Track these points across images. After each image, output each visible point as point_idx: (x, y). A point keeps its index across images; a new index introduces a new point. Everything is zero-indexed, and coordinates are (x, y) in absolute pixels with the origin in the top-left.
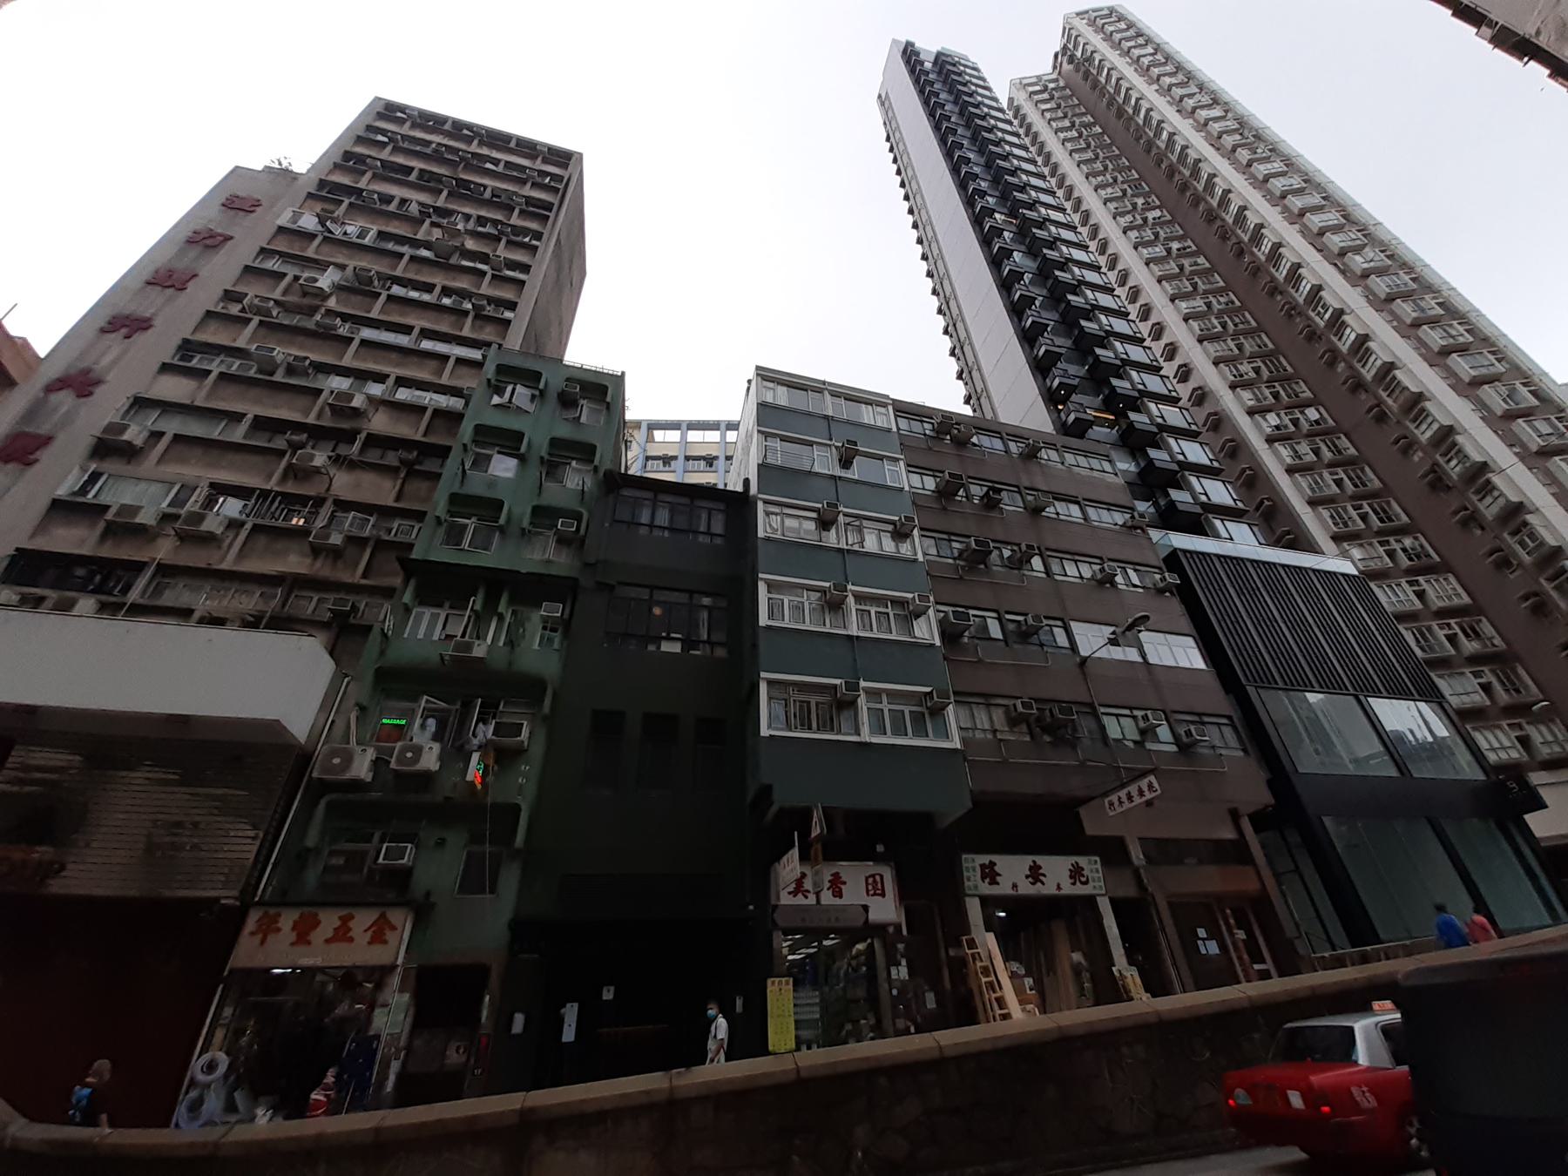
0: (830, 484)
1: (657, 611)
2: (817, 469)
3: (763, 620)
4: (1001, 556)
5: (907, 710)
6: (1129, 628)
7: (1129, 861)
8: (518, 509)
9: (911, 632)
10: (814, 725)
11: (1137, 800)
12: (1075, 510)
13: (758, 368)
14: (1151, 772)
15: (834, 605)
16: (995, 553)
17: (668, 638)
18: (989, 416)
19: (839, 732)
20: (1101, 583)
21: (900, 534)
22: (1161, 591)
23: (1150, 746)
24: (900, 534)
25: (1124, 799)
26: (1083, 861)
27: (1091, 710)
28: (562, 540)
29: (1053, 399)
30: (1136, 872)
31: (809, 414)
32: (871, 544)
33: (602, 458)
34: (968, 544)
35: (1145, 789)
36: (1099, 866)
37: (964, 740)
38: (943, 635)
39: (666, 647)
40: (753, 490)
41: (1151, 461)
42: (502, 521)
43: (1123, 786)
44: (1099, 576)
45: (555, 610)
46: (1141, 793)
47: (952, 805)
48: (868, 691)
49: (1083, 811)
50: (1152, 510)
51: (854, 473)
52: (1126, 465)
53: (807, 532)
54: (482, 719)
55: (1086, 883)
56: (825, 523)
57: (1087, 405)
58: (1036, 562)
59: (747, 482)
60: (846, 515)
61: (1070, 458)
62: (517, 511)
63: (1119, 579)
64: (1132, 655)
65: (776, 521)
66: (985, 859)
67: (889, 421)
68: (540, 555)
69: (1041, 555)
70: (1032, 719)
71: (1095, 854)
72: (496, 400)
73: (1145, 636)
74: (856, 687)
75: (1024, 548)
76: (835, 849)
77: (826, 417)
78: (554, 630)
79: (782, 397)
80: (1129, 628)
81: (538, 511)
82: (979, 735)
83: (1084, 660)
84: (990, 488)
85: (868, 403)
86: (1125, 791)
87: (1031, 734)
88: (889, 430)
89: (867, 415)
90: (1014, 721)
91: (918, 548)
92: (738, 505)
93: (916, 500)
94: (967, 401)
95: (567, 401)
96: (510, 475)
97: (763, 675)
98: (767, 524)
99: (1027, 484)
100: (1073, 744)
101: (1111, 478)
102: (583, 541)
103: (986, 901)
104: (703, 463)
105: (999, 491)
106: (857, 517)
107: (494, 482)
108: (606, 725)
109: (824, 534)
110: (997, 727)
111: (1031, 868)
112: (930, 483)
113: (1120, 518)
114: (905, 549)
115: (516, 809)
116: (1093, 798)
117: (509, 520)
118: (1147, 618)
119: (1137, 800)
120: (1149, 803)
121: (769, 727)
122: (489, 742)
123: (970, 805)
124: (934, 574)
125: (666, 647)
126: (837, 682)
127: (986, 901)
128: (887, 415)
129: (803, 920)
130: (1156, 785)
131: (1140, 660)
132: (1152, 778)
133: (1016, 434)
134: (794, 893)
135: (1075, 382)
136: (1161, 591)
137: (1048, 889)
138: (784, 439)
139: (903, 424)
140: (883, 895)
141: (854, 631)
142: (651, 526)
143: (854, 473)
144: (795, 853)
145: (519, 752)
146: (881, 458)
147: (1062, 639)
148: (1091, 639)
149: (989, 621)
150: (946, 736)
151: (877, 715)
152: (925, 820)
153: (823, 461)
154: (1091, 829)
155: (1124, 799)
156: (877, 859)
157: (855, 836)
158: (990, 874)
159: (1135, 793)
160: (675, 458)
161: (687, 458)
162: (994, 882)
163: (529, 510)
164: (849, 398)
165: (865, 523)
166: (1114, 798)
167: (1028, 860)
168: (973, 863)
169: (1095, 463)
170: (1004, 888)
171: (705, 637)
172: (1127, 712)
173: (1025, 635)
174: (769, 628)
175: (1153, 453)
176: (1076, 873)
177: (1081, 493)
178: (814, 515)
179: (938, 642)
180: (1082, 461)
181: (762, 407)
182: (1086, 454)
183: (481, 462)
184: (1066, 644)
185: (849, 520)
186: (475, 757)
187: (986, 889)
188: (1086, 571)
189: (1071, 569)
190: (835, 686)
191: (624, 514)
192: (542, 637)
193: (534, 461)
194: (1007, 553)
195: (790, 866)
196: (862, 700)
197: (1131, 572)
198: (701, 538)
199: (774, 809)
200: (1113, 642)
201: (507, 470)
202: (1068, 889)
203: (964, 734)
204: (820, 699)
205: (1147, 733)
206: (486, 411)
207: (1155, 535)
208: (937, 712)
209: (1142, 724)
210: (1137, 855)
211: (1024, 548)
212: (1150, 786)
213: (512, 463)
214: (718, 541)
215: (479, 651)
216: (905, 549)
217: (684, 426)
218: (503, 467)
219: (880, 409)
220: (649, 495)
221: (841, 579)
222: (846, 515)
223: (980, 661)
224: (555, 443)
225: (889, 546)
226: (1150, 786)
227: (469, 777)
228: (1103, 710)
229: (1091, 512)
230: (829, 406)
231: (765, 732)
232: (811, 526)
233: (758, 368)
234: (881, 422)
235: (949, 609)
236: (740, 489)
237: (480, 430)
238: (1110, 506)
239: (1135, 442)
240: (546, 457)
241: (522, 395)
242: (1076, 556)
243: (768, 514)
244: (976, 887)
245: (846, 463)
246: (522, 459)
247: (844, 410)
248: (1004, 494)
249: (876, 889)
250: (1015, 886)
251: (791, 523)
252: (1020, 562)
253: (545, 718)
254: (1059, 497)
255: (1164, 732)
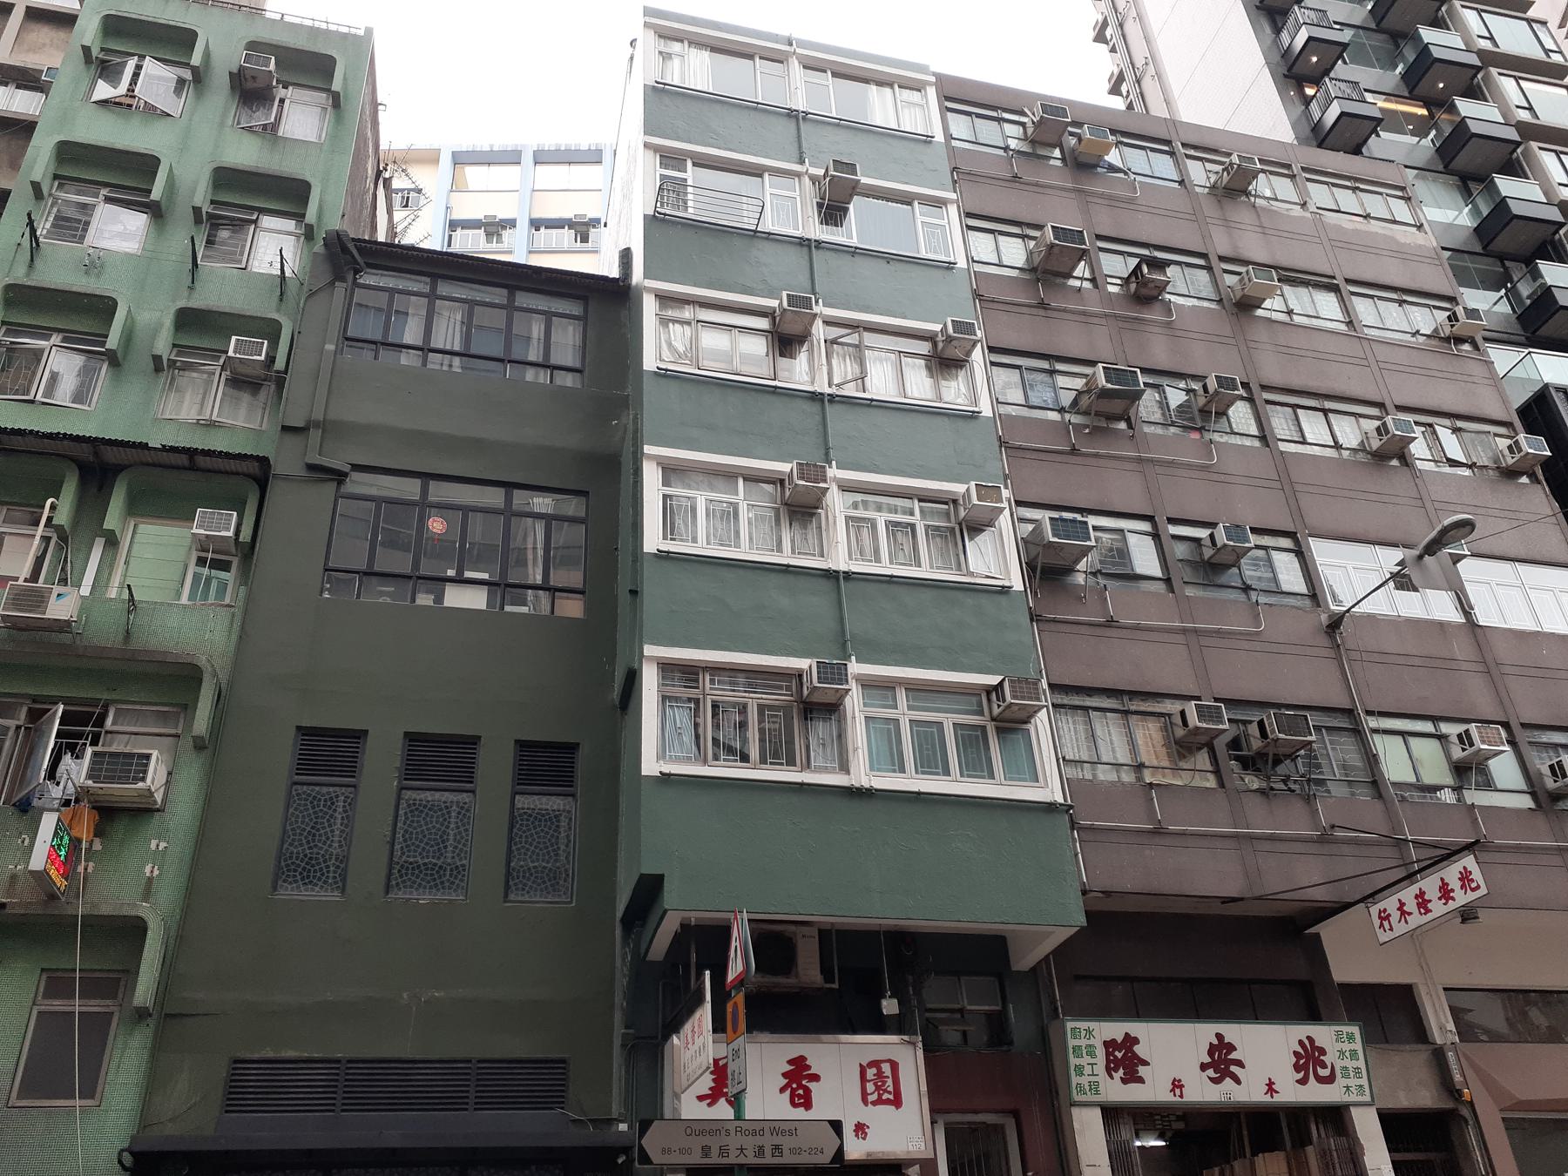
0: (796, 257)
1: (436, 525)
2: (768, 225)
3: (653, 539)
4: (1164, 404)
5: (948, 721)
6: (1432, 548)
7: (1421, 1034)
8: (148, 315)
9: (960, 564)
10: (754, 753)
11: (1438, 908)
12: (1327, 305)
13: (648, 12)
14: (1469, 847)
15: (801, 509)
16: (1150, 397)
17: (460, 580)
18: (1158, 109)
19: (807, 766)
20: (1380, 457)
21: (945, 361)
22: (1510, 474)
23: (1475, 797)
24: (945, 361)
25: (1411, 906)
26: (1323, 1034)
27: (1348, 720)
28: (242, 381)
29: (1298, 74)
30: (1439, 1055)
31: (756, 108)
32: (881, 383)
33: (330, 207)
34: (1090, 379)
35: (1454, 884)
36: (1358, 1045)
37: (1069, 785)
38: (1032, 569)
39: (456, 598)
40: (637, 275)
41: (1501, 205)
42: (113, 342)
43: (1410, 877)
44: (1375, 444)
45: (223, 525)
46: (1446, 893)
47: (1044, 920)
48: (868, 684)
49: (1328, 932)
50: (1504, 308)
51: (850, 233)
52: (1450, 214)
53: (745, 358)
54: (69, 744)
55: (1330, 1079)
56: (786, 341)
57: (1367, 84)
58: (1240, 414)
59: (626, 256)
60: (828, 322)
61: (1320, 195)
62: (145, 317)
63: (1419, 449)
64: (1438, 606)
65: (679, 336)
66: (1115, 1030)
67: (928, 121)
68: (193, 411)
69: (1250, 400)
70: (1220, 744)
71: (1352, 1019)
72: (103, 90)
73: (1469, 569)
74: (839, 674)
75: (1212, 384)
76: (775, 1009)
77: (792, 114)
78: (225, 566)
79: (696, 71)
80: (1432, 548)
81: (189, 320)
82: (1105, 775)
83: (1336, 623)
84: (1144, 259)
85: (883, 82)
86: (1414, 889)
87: (1217, 772)
88: (927, 140)
89: (881, 108)
90: (1184, 746)
91: (981, 388)
92: (606, 301)
93: (984, 293)
94: (1115, 90)
95: (251, 91)
96: (132, 246)
97: (649, 650)
98: (661, 344)
99: (1224, 249)
100: (1309, 789)
101: (1407, 236)
102: (280, 383)
103: (1112, 1114)
104: (567, 235)
105: (1160, 265)
106: (854, 326)
107: (94, 265)
108: (328, 752)
109: (783, 362)
110: (1145, 758)
111: (1212, 1050)
112: (1015, 252)
113: (1425, 319)
114: (954, 392)
115: (135, 930)
116: (1347, 906)
117: (128, 336)
118: (1466, 526)
119: (1438, 908)
120: (1467, 915)
121: (661, 756)
122: (82, 794)
123: (1082, 920)
124: (1013, 442)
125: (456, 598)
126: (803, 663)
127: (1112, 1114)
128: (924, 107)
129: (706, 1151)
130: (1477, 875)
131: (1457, 617)
132: (1469, 862)
133: (1203, 147)
134: (712, 1098)
135: (1346, 36)
136: (1510, 474)
137: (1248, 1091)
138: (702, 162)
139: (960, 126)
140: (897, 1102)
141: (840, 560)
142: (425, 349)
143: (850, 233)
144: (705, 1014)
145: (143, 811)
146: (906, 199)
147: (1289, 575)
148: (1354, 575)
149: (1132, 539)
150: (1034, 776)
151: (886, 731)
152: (983, 954)
153: (786, 209)
154: (1347, 967)
155: (1411, 906)
156: (879, 1025)
157: (831, 980)
158: (1125, 1060)
159: (1432, 893)
160: (512, 223)
161: (536, 224)
162: (1132, 1077)
163: (168, 321)
164: (841, 74)
165: (869, 339)
166: (1390, 904)
167: (1205, 1032)
168: (1087, 1039)
169: (1375, 204)
170: (1153, 1090)
171: (539, 580)
172: (1427, 727)
173: (1213, 567)
174: (664, 556)
175: (1506, 186)
176: (1309, 1060)
177: (1344, 267)
178: (763, 324)
179: (1017, 584)
180: (1347, 200)
181: (660, 95)
182: (1356, 183)
183: (73, 226)
184: (1301, 587)
185: (835, 332)
186: (49, 822)
187: (1117, 1091)
188: (1349, 432)
189: (1314, 427)
190: (799, 675)
191: (367, 326)
192: (197, 577)
193: (183, 214)
194: (1176, 397)
195: (695, 1044)
196: (854, 702)
197: (1445, 434)
198: (530, 375)
199: (669, 927)
200: (1402, 581)
201: (123, 236)
202: (1291, 1092)
203: (1070, 772)
204: (768, 698)
205: (1469, 771)
206: (71, 112)
207: (1503, 358)
208: (1012, 725)
209: (1457, 753)
210: (1440, 1023)
211: (1212, 384)
212: (1465, 878)
213: (137, 221)
214: (568, 380)
215: (62, 607)
216: (954, 392)
217: (527, 158)
218: (118, 230)
219: (907, 95)
220: (418, 285)
221: (817, 458)
222: (828, 322)
223: (1110, 623)
224: (225, 178)
225: (919, 386)
226: (1465, 878)
227: (38, 861)
228: (1373, 723)
229: (1364, 309)
230: (798, 90)
231: (651, 765)
232: (757, 346)
233: (648, 12)
234: (912, 122)
235: (1044, 516)
236: (614, 272)
237: (70, 154)
238: (1404, 294)
239: (1468, 162)
240: (206, 208)
241: (155, 79)
242: (1326, 401)
243: (664, 322)
244: (1094, 1087)
245: (833, 212)
246: (156, 211)
247: (831, 99)
248: (1171, 271)
249: (880, 1086)
250: (1177, 1085)
251: (712, 340)
252: (1205, 413)
253: (199, 745)
254: (1294, 277)
255: (1504, 768)
